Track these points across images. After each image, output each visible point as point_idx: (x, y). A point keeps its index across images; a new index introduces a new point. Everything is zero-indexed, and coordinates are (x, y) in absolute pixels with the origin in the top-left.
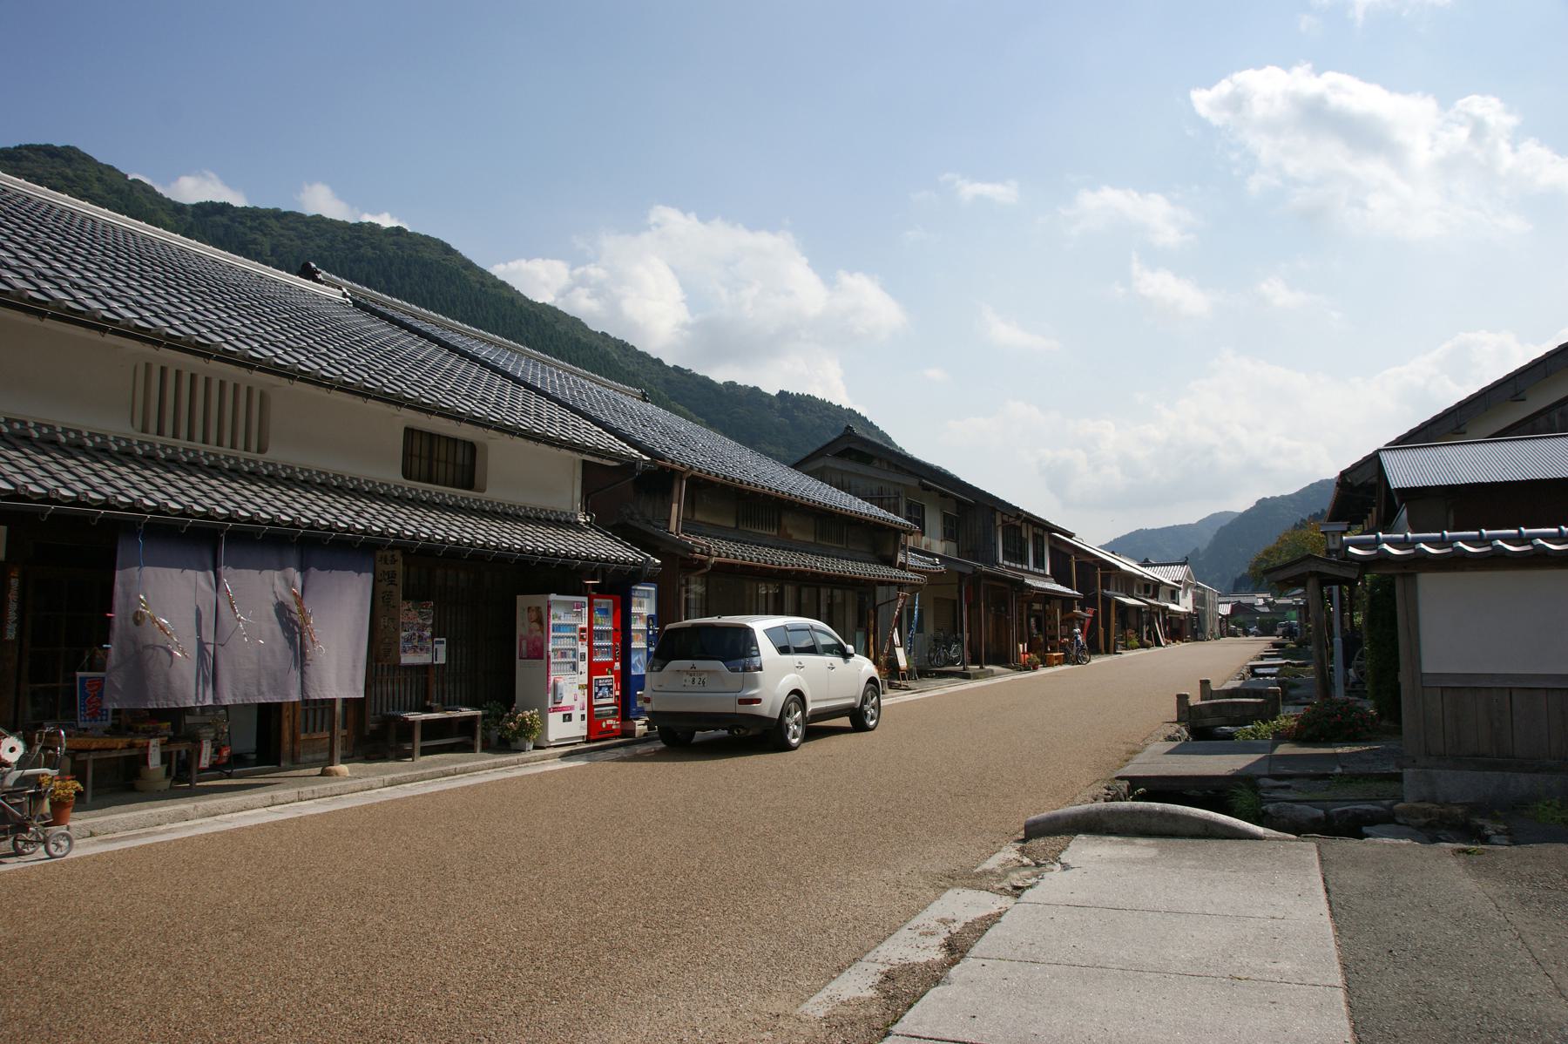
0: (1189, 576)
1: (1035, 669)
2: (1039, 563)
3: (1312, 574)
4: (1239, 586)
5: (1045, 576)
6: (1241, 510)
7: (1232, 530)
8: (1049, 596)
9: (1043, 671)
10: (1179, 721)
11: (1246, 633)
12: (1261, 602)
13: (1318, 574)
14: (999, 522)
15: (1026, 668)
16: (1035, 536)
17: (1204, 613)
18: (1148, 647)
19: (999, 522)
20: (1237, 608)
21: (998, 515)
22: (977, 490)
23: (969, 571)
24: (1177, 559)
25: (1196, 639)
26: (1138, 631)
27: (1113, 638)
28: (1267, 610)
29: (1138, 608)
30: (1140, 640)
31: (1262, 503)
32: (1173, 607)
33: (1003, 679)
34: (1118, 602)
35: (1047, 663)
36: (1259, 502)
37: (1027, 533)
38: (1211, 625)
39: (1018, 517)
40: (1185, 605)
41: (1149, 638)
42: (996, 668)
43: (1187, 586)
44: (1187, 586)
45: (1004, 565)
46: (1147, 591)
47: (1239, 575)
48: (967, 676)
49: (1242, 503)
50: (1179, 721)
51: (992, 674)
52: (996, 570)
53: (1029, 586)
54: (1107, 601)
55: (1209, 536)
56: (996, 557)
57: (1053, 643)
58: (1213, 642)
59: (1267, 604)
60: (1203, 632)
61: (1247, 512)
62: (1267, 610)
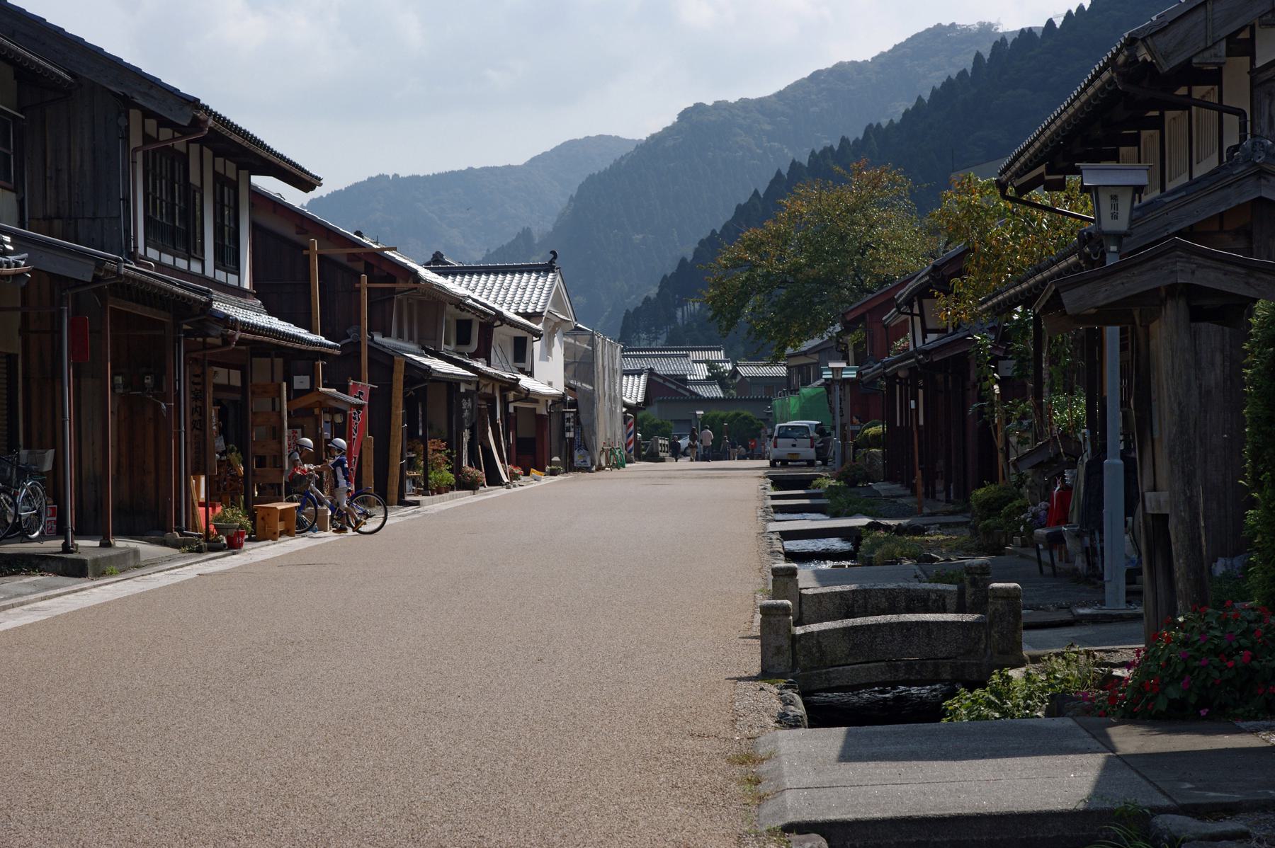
0: (557, 302)
1: (234, 546)
2: (228, 259)
3: (1174, 291)
4: (638, 328)
5: (238, 291)
6: (642, 134)
7: (615, 184)
8: (263, 346)
9: (257, 553)
10: (766, 674)
11: (676, 453)
12: (702, 372)
13: (1190, 292)
14: (136, 140)
15: (210, 545)
16: (220, 180)
17: (591, 399)
18: (472, 486)
19: (136, 140)
20: (656, 385)
21: (135, 115)
22: (58, 33)
23: (85, 273)
24: (540, 259)
25: (570, 467)
26: (453, 443)
27: (396, 462)
28: (716, 392)
29: (451, 383)
30: (457, 469)
31: (693, 117)
32: (525, 382)
33: (162, 577)
34: (410, 365)
35: (261, 533)
36: (684, 115)
37: (202, 170)
38: (609, 429)
39: (196, 124)
40: (546, 377)
41: (473, 460)
42: (146, 549)
43: (555, 326)
44: (555, 326)
45: (151, 259)
46: (463, 339)
47: (634, 301)
48: (77, 569)
49: (639, 111)
50: (766, 674)
51: (129, 564)
52: (129, 268)
53: (226, 320)
54: (383, 362)
55: (558, 198)
56: (129, 237)
57: (269, 474)
58: (607, 473)
59: (716, 377)
60: (587, 446)
61: (656, 140)
62: (716, 392)
